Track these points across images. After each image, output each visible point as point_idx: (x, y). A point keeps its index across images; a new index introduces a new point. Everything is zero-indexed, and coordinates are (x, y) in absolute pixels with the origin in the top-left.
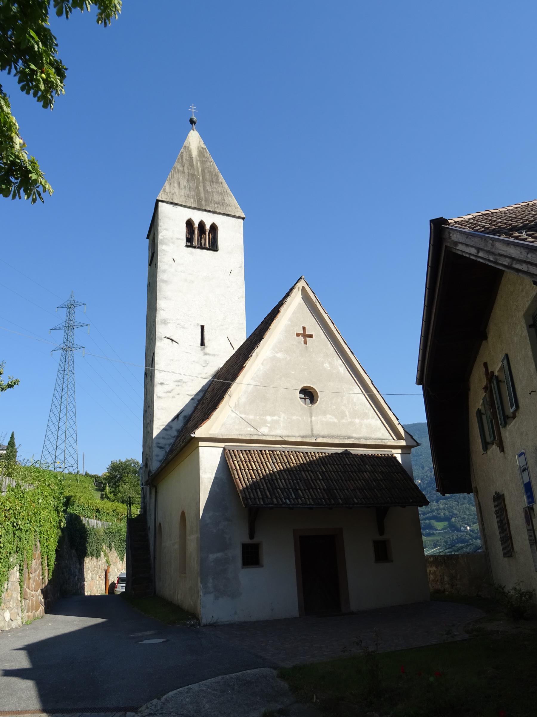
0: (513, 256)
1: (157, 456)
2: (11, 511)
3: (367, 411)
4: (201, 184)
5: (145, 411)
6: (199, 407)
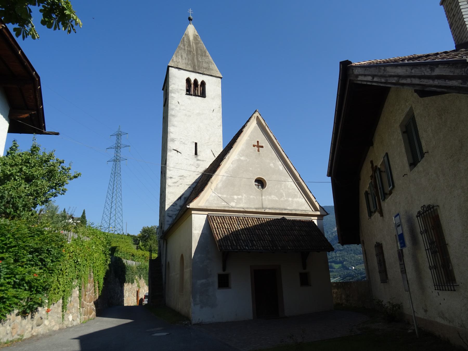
0: (400, 74)
1: (168, 221)
2: (73, 253)
4: (196, 57)
5: (161, 195)
6: (194, 192)
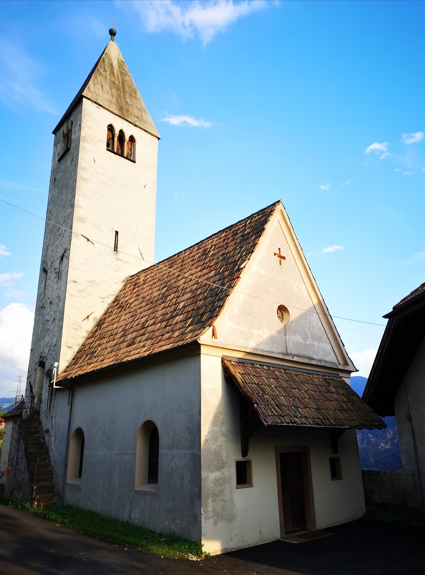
3: (322, 335)
